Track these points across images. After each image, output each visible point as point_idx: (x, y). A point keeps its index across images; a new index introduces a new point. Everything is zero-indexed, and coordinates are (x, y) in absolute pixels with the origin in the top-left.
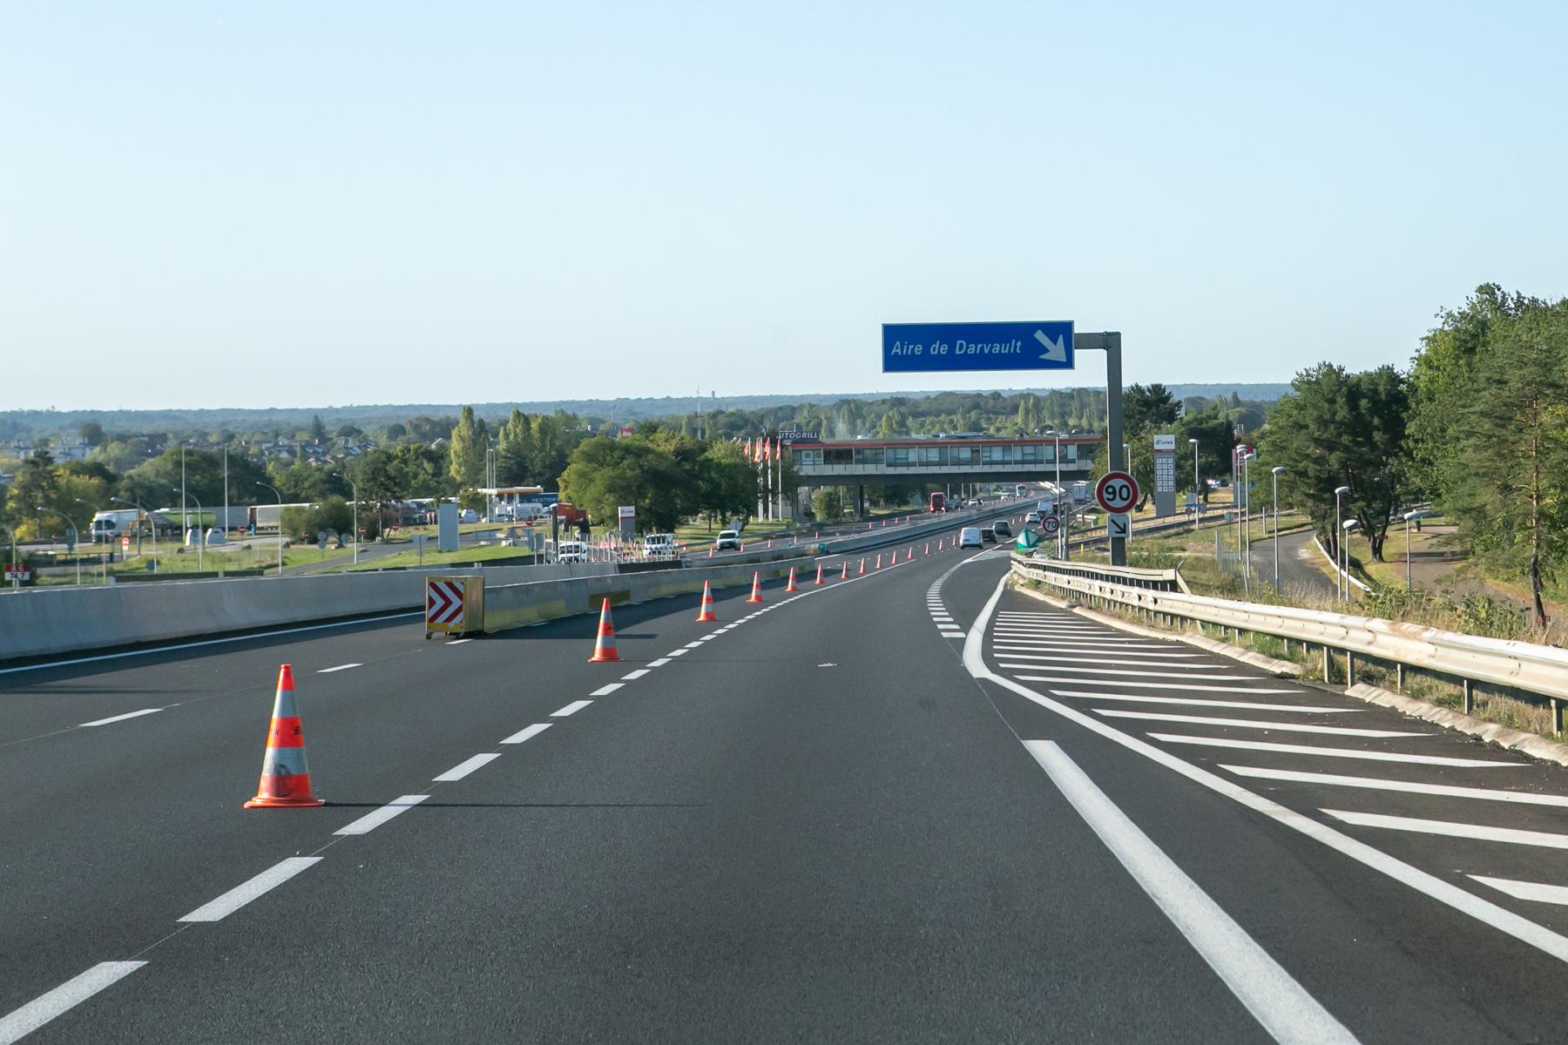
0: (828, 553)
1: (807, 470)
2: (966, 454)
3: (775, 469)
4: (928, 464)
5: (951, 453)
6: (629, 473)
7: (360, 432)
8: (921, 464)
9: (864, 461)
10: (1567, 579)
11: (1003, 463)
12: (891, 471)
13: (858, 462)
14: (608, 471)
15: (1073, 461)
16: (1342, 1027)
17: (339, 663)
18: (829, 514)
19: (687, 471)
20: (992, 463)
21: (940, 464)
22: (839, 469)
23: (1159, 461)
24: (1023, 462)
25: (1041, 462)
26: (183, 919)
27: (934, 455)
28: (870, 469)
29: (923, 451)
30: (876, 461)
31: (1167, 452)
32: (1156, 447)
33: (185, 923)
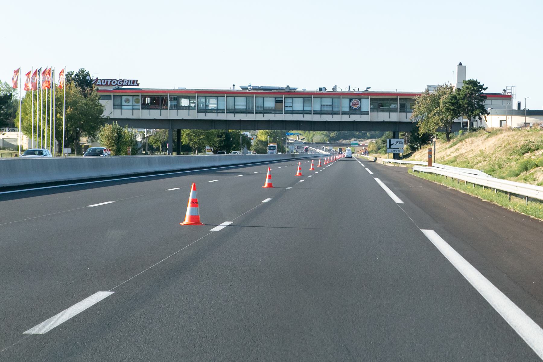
2: (270, 103)
4: (235, 111)
5: (258, 102)
8: (229, 111)
10: (1, 94)
11: (303, 112)
15: (367, 113)
16: (520, 310)
20: (293, 112)
21: (246, 111)
22: (155, 114)
24: (321, 113)
25: (337, 113)
26: (26, 332)
27: (241, 103)
29: (231, 100)
33: (26, 334)
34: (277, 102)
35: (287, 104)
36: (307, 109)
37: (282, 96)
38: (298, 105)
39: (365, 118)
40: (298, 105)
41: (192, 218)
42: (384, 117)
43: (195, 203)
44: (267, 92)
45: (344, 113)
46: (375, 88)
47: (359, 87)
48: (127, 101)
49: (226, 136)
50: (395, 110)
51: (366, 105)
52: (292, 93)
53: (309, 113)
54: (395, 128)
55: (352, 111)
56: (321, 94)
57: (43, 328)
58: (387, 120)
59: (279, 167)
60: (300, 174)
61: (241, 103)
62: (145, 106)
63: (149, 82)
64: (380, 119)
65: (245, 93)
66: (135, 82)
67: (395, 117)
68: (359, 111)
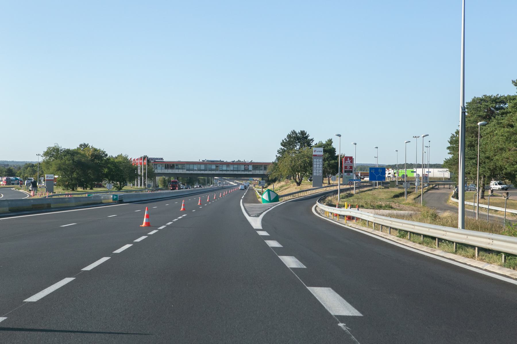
0: (121, 202)
1: (158, 171)
2: (214, 167)
3: (145, 169)
5: (209, 166)
6: (67, 162)
7: (420, 244)
8: (198, 170)
9: (178, 169)
11: (226, 171)
12: (188, 172)
13: (177, 169)
14: (58, 161)
15: (251, 171)
17: (155, 206)
18: (164, 186)
19: (96, 163)
20: (222, 170)
22: (170, 171)
23: (315, 160)
24: (233, 171)
25: (240, 171)
26: (25, 301)
27: (203, 167)
28: (181, 171)
29: (199, 166)
30: (182, 169)
31: (319, 156)
32: (314, 153)
33: (25, 302)
34: (216, 166)
35: (220, 167)
36: (228, 169)
37: (218, 164)
38: (225, 168)
39: (250, 173)
40: (225, 168)
41: (146, 223)
42: (257, 172)
43: (148, 216)
44: (212, 162)
45: (242, 171)
46: (255, 161)
47: (248, 160)
48: (159, 166)
49: (191, 179)
50: (262, 170)
51: (251, 168)
52: (222, 163)
53: (229, 171)
54: (262, 176)
55: (245, 170)
56: (233, 163)
57: (35, 298)
58: (259, 173)
59: (190, 199)
60: (184, 209)
61: (203, 167)
62: (166, 168)
63: (167, 159)
64: (256, 173)
65: (203, 163)
66: (162, 159)
67: (261, 172)
68: (248, 170)
